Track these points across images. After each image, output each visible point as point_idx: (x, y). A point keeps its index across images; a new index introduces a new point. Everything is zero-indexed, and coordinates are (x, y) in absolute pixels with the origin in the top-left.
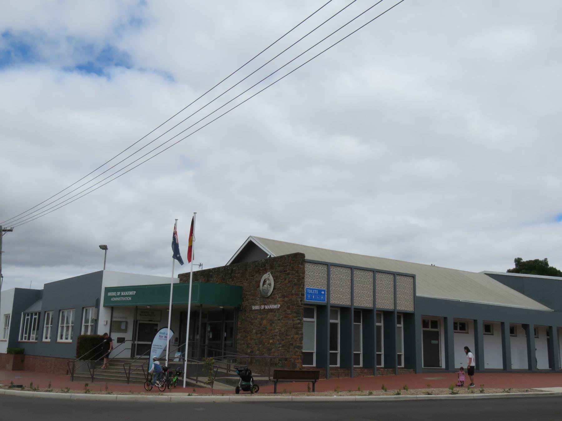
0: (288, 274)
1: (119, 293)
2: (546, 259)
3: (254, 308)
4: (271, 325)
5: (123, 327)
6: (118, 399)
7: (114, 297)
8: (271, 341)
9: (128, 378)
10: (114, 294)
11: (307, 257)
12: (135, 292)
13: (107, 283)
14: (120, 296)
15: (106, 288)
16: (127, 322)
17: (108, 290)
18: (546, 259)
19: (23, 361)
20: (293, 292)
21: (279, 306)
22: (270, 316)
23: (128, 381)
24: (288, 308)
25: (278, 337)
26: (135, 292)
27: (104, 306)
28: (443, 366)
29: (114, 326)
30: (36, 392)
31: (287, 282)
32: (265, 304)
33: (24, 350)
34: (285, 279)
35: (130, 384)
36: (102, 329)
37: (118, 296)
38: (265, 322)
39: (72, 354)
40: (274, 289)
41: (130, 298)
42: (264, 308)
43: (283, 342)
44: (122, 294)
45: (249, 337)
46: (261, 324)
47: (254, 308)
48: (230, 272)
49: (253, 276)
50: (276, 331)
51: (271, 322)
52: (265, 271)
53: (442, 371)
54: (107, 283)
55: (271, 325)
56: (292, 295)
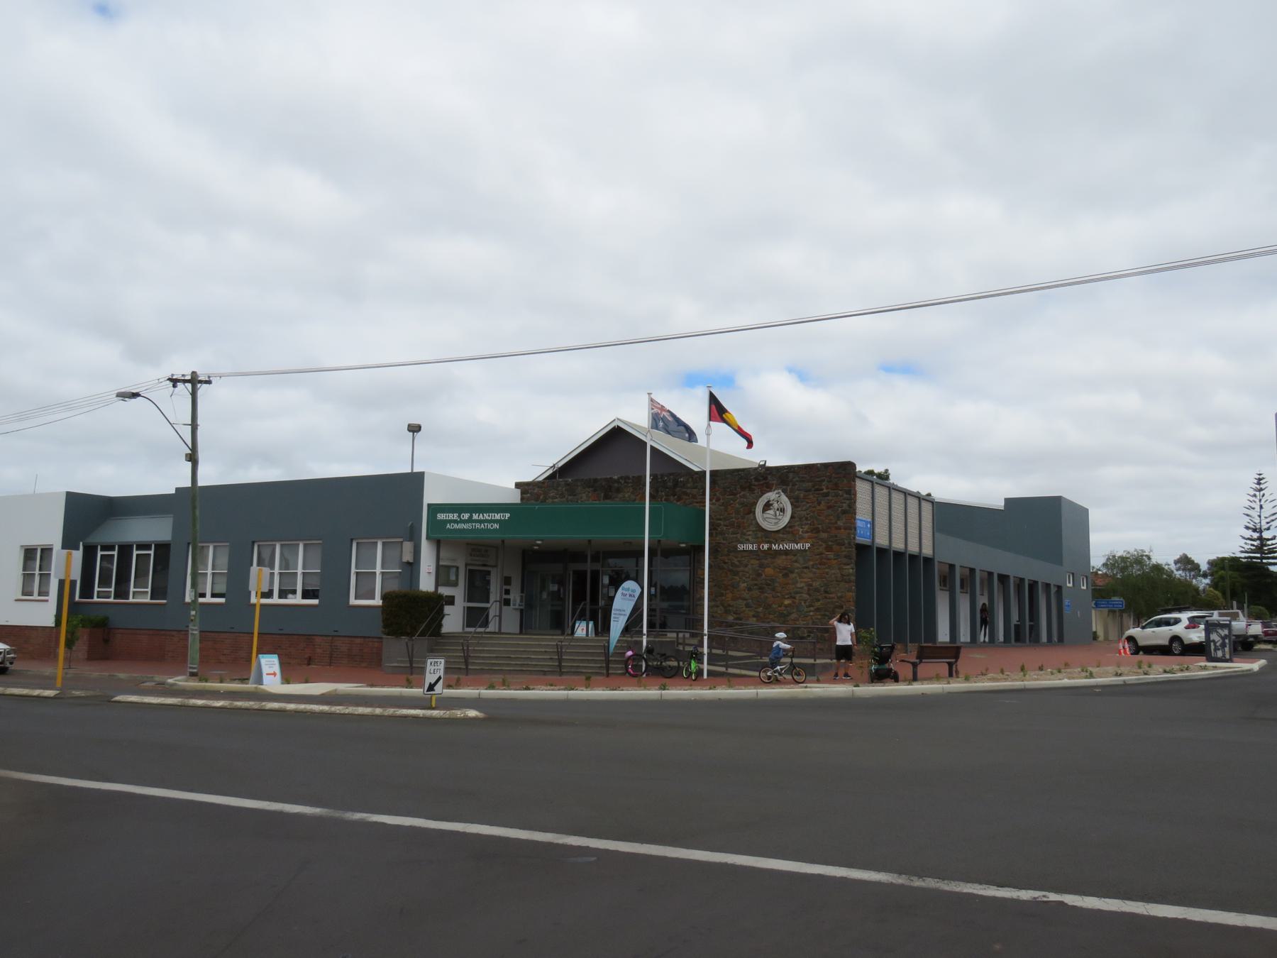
0: (827, 495)
1: (466, 516)
2: (887, 471)
3: (741, 547)
4: (786, 575)
5: (453, 578)
6: (761, 696)
7: (455, 521)
8: (787, 602)
9: (560, 666)
10: (451, 516)
11: (861, 468)
12: (508, 515)
13: (432, 496)
14: (470, 520)
15: (429, 505)
16: (457, 568)
17: (434, 509)
18: (887, 471)
19: (106, 641)
20: (840, 523)
21: (808, 545)
22: (781, 561)
23: (561, 673)
24: (829, 549)
25: (805, 596)
26: (508, 515)
27: (428, 538)
28: (1001, 638)
29: (442, 575)
30: (1187, 674)
31: (823, 506)
32: (771, 543)
33: (107, 618)
34: (819, 504)
35: (564, 677)
36: (426, 583)
37: (464, 522)
38: (769, 571)
39: (377, 627)
40: (792, 517)
41: (496, 526)
42: (770, 549)
43: (818, 604)
44: (475, 517)
45: (730, 595)
46: (759, 575)
47: (741, 547)
48: (670, 484)
49: (735, 495)
50: (799, 585)
51: (787, 572)
52: (769, 488)
53: (1043, 645)
54: (432, 496)
55: (786, 575)
56: (838, 528)
